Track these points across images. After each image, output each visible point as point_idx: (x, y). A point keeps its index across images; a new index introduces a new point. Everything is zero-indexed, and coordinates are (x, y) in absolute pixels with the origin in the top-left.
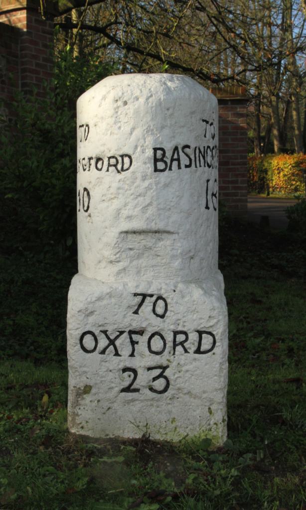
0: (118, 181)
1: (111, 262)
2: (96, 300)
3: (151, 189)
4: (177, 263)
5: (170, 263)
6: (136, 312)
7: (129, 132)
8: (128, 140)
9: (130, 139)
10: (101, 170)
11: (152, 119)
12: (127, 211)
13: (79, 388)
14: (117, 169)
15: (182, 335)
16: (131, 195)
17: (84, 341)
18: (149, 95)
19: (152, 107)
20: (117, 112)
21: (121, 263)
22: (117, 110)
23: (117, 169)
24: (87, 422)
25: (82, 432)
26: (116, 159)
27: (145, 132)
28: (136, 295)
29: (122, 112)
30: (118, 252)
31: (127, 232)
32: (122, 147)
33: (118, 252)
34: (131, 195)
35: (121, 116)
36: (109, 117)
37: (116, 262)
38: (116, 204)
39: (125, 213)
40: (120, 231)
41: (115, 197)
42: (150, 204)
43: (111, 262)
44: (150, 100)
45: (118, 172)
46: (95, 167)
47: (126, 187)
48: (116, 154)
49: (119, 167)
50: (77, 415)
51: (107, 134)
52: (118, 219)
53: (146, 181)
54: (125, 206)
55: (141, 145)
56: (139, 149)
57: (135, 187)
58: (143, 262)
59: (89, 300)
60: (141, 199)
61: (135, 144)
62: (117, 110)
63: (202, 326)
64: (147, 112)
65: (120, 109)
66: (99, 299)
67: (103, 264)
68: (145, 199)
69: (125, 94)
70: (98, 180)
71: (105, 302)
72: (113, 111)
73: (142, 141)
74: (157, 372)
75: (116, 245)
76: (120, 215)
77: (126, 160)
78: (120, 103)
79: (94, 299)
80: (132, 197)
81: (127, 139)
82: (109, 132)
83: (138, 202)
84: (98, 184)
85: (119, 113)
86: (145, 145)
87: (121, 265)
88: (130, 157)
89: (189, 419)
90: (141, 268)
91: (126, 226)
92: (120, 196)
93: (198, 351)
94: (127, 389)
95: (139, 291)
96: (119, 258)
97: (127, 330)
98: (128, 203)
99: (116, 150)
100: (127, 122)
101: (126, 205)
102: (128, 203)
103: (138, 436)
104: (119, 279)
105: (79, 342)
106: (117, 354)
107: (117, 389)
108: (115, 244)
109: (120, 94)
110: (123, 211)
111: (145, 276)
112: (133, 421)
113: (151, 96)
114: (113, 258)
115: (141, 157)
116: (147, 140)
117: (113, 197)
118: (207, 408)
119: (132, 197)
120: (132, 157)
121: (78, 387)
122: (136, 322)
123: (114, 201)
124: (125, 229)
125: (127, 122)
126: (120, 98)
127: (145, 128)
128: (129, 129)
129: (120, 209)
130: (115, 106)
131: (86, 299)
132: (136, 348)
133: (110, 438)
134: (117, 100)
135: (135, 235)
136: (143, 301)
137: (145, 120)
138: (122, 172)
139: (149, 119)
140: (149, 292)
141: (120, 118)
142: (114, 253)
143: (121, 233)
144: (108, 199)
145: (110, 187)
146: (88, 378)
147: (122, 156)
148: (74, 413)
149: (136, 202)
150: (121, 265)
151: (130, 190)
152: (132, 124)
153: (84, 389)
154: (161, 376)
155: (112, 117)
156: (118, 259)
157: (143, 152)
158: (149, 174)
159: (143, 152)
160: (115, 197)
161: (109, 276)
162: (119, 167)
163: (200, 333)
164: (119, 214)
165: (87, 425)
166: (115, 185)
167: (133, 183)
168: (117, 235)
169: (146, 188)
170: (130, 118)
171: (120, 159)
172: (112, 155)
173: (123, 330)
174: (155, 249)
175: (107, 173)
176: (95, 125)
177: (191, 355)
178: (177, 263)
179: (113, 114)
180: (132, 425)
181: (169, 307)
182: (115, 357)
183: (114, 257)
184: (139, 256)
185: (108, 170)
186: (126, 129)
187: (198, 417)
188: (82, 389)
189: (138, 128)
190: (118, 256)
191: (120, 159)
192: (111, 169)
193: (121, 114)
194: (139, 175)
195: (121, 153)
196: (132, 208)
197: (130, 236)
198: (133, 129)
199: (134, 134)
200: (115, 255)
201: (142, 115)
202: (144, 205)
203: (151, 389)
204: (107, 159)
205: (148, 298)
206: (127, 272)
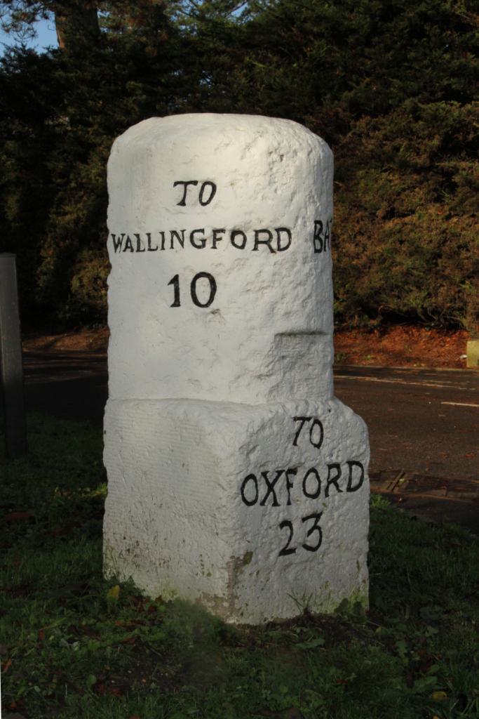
0: (273, 264)
1: (260, 377)
2: (258, 430)
3: (312, 275)
4: (327, 374)
5: (321, 374)
6: (295, 444)
7: (290, 197)
8: (287, 208)
9: (290, 206)
10: (242, 247)
11: (314, 183)
12: (284, 305)
13: (238, 558)
14: (270, 248)
15: (249, 482)
16: (291, 283)
17: (245, 490)
18: (310, 149)
19: (314, 166)
20: (271, 169)
21: (273, 377)
22: (271, 166)
23: (270, 248)
24: (247, 605)
25: (243, 621)
26: (269, 232)
27: (307, 199)
28: (296, 419)
29: (278, 170)
30: (270, 363)
31: (282, 335)
32: (280, 218)
33: (270, 363)
34: (291, 283)
35: (277, 174)
36: (260, 174)
37: (267, 376)
38: (269, 296)
39: (281, 308)
40: (276, 333)
41: (269, 286)
42: (310, 296)
43: (260, 377)
44: (311, 155)
45: (272, 251)
46: (190, 243)
47: (284, 272)
48: (271, 226)
49: (274, 245)
50: (237, 597)
51: (256, 198)
52: (273, 316)
53: (306, 265)
54: (282, 299)
55: (302, 215)
56: (300, 221)
57: (296, 273)
58: (296, 374)
59: (251, 430)
60: (300, 289)
61: (296, 215)
62: (271, 166)
63: (354, 454)
64: (310, 173)
65: (276, 164)
66: (263, 427)
67: (244, 381)
68: (305, 289)
69: (282, 145)
70: (238, 261)
71: (267, 431)
72: (266, 168)
73: (303, 210)
74: (311, 522)
75: (271, 352)
76: (275, 311)
77: (284, 235)
78: (275, 157)
79: (256, 429)
80: (291, 285)
81: (286, 206)
82: (260, 196)
83: (298, 293)
84: (239, 267)
85: (274, 170)
86: (306, 217)
87: (274, 380)
88: (288, 231)
89: (340, 581)
90: (294, 382)
91: (284, 326)
92: (276, 284)
93: (350, 489)
94: (285, 552)
95: (298, 415)
96: (272, 369)
97: (286, 469)
98: (287, 294)
99: (271, 222)
100: (285, 184)
101: (283, 297)
102: (287, 294)
103: (298, 612)
104: (272, 400)
105: (240, 492)
106: (275, 504)
107: (277, 552)
108: (269, 351)
109: (276, 144)
110: (279, 306)
111: (299, 392)
112: (291, 594)
113: (311, 151)
114: (264, 370)
115: (303, 232)
116: (308, 210)
117: (265, 285)
118: (356, 561)
119: (291, 285)
120: (292, 232)
121: (236, 556)
122: (289, 456)
123: (265, 291)
124: (282, 330)
125: (285, 184)
126: (276, 150)
127: (307, 193)
128: (290, 193)
129: (277, 302)
130: (270, 160)
131: (247, 430)
132: (291, 493)
133: (270, 623)
134: (271, 153)
135: (289, 339)
136: (302, 424)
137: (307, 183)
138: (278, 252)
139: (312, 181)
140: (308, 415)
141: (275, 178)
142: (267, 364)
143: (276, 335)
144: (257, 289)
145: (260, 272)
146: (249, 542)
147: (278, 230)
148: (232, 595)
149: (296, 293)
150: (274, 380)
151: (289, 276)
152: (292, 187)
153: (244, 558)
154: (316, 527)
155: (265, 175)
156: (271, 372)
157: (305, 226)
158: (309, 255)
159: (304, 225)
160: (269, 286)
161: (257, 396)
162: (274, 245)
163: (351, 463)
164: (273, 309)
165: (247, 610)
166: (269, 269)
167: (293, 266)
168: (272, 339)
169: (307, 273)
170: (291, 178)
171: (274, 234)
172: (264, 228)
173: (280, 469)
174: (309, 356)
175: (254, 252)
176: (232, 184)
177: (345, 494)
178: (327, 374)
179: (267, 172)
180: (291, 598)
181: (325, 432)
182: (274, 508)
183: (266, 370)
184: (291, 367)
185: (255, 249)
186: (284, 192)
187: (348, 575)
188: (242, 558)
189: (299, 192)
190: (270, 367)
191: (274, 234)
192: (261, 246)
193: (277, 172)
194: (300, 257)
195: (278, 225)
196: (291, 301)
197: (284, 339)
198: (294, 194)
199: (294, 200)
200: (267, 366)
201: (304, 176)
202: (304, 298)
203: (306, 547)
204: (254, 233)
205: (306, 422)
206: (280, 389)
